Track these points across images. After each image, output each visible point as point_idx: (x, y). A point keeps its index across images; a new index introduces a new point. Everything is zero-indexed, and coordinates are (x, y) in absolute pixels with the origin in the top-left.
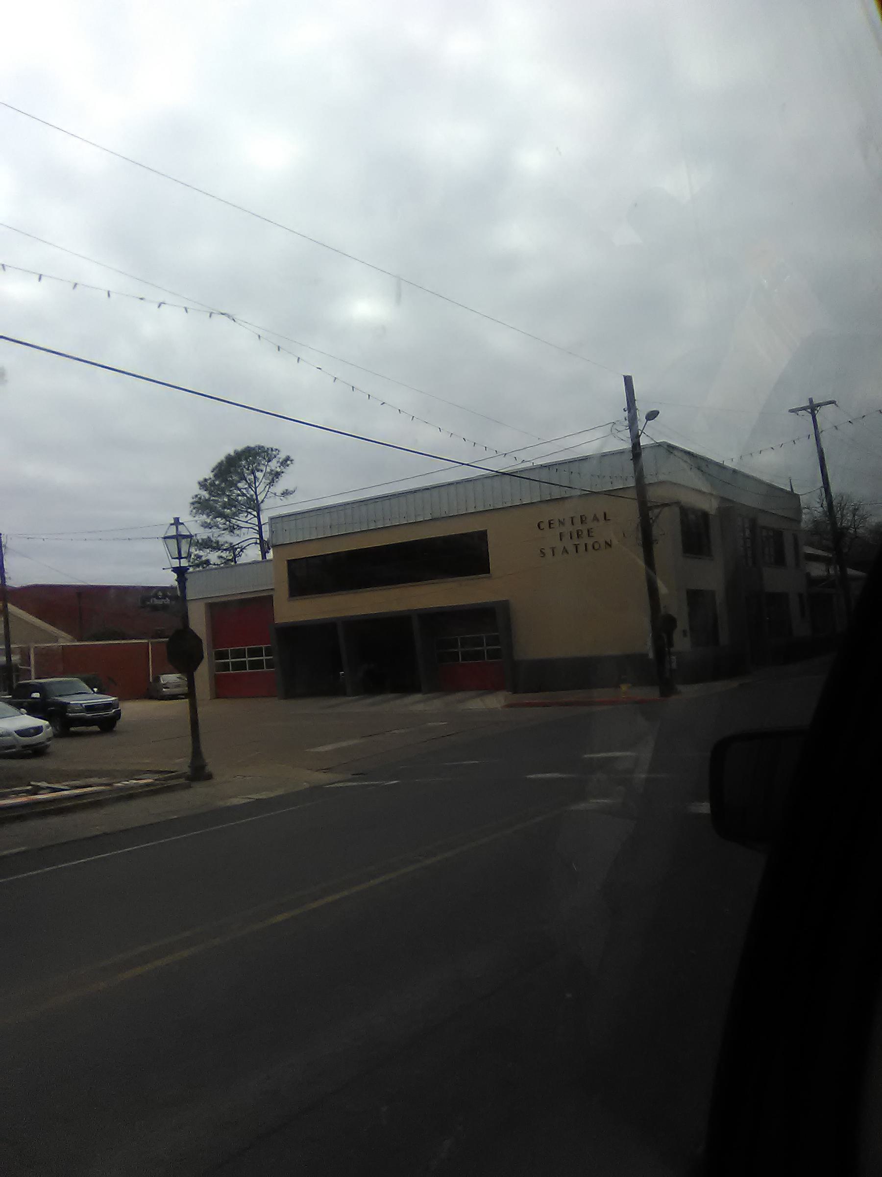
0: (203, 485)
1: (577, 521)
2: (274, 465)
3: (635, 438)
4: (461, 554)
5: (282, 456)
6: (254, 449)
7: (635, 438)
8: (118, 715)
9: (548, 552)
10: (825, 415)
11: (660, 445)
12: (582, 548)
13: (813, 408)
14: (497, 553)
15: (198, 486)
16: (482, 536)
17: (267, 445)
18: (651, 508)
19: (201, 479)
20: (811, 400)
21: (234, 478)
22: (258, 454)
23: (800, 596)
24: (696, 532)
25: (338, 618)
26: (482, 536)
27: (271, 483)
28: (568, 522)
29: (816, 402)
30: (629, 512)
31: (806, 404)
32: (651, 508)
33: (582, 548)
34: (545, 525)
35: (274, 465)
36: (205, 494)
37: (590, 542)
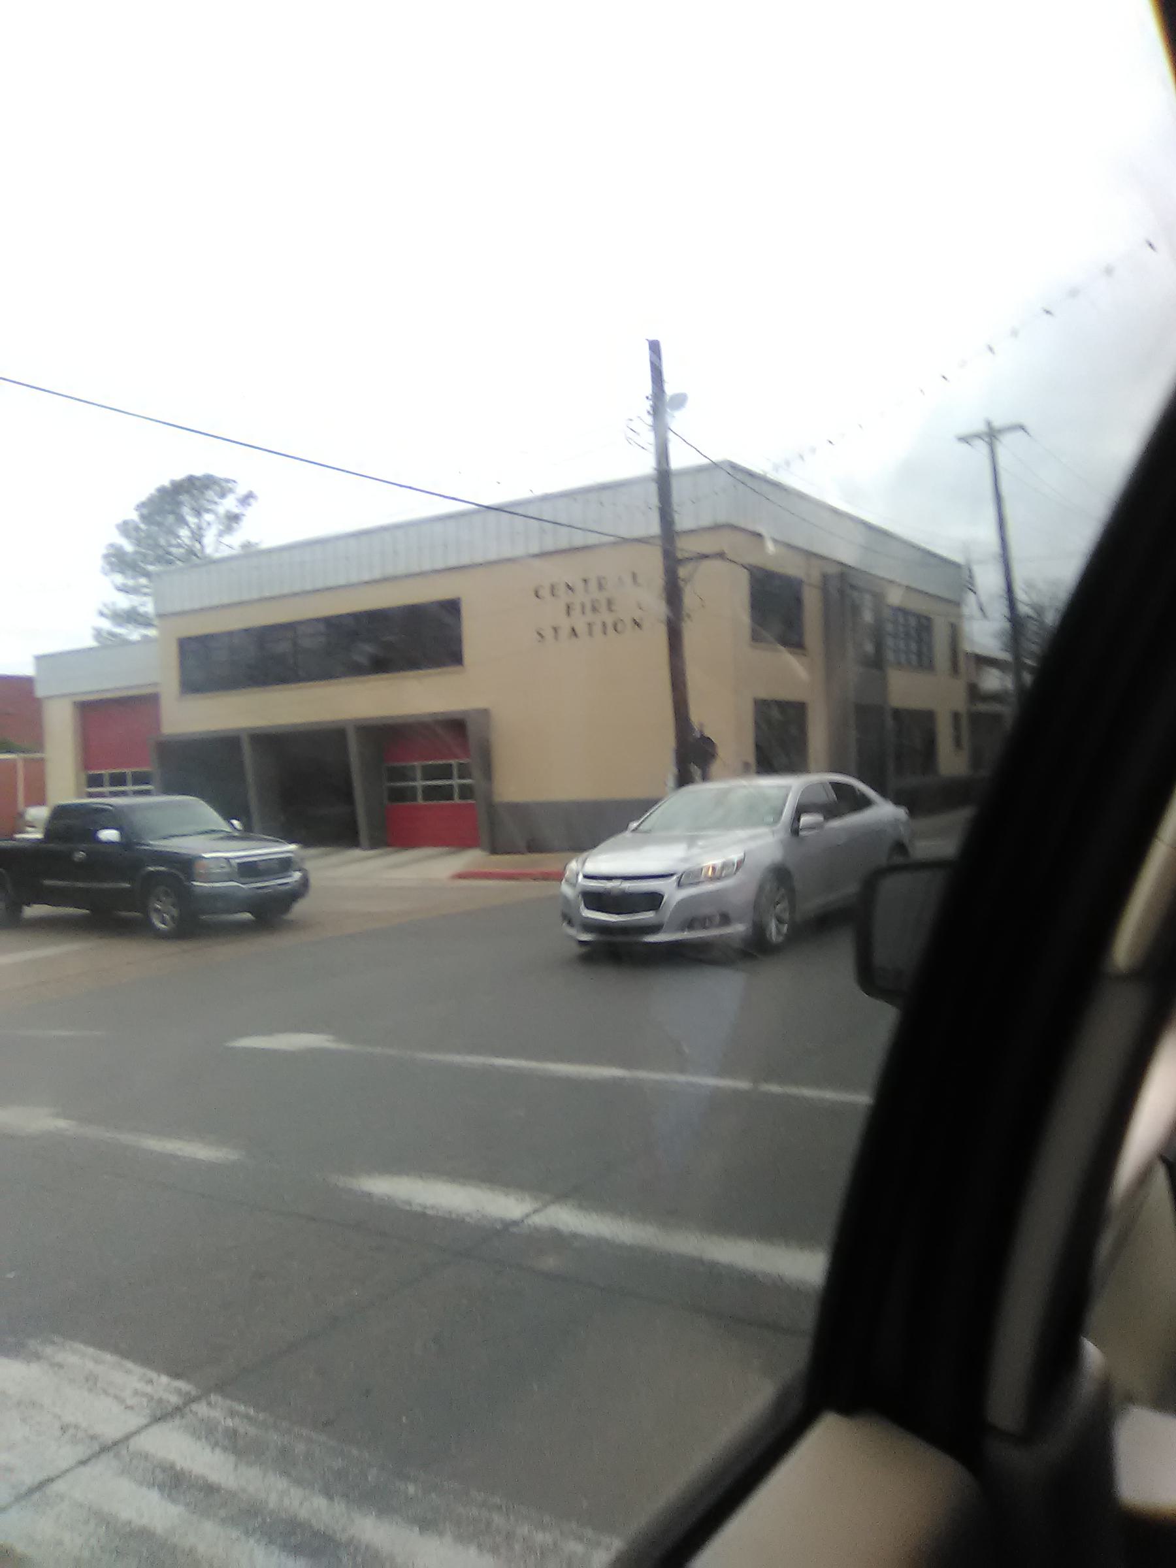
0: (126, 528)
1: (593, 585)
2: (229, 504)
3: (663, 454)
4: (418, 635)
5: (241, 491)
6: (198, 479)
7: (663, 454)
8: (304, 885)
9: (548, 634)
10: (1007, 447)
11: (715, 466)
12: (598, 629)
13: (991, 435)
14: (475, 634)
15: (116, 532)
16: (452, 607)
17: (219, 473)
18: (680, 562)
19: (120, 521)
20: (989, 424)
21: (689, 616)
22: (207, 487)
23: (956, 716)
24: (776, 605)
25: (244, 730)
26: (452, 607)
27: (229, 529)
28: (579, 586)
29: (998, 423)
30: (653, 565)
31: (981, 427)
32: (680, 562)
33: (598, 629)
34: (545, 592)
35: (229, 504)
36: (128, 547)
37: (609, 619)
